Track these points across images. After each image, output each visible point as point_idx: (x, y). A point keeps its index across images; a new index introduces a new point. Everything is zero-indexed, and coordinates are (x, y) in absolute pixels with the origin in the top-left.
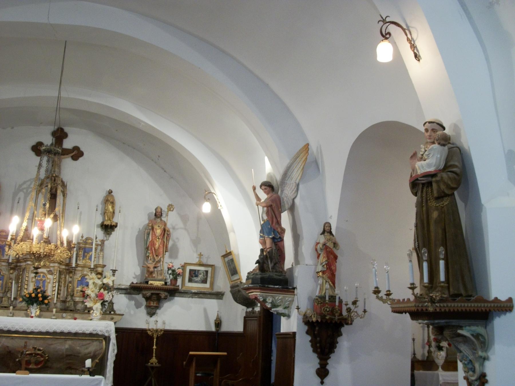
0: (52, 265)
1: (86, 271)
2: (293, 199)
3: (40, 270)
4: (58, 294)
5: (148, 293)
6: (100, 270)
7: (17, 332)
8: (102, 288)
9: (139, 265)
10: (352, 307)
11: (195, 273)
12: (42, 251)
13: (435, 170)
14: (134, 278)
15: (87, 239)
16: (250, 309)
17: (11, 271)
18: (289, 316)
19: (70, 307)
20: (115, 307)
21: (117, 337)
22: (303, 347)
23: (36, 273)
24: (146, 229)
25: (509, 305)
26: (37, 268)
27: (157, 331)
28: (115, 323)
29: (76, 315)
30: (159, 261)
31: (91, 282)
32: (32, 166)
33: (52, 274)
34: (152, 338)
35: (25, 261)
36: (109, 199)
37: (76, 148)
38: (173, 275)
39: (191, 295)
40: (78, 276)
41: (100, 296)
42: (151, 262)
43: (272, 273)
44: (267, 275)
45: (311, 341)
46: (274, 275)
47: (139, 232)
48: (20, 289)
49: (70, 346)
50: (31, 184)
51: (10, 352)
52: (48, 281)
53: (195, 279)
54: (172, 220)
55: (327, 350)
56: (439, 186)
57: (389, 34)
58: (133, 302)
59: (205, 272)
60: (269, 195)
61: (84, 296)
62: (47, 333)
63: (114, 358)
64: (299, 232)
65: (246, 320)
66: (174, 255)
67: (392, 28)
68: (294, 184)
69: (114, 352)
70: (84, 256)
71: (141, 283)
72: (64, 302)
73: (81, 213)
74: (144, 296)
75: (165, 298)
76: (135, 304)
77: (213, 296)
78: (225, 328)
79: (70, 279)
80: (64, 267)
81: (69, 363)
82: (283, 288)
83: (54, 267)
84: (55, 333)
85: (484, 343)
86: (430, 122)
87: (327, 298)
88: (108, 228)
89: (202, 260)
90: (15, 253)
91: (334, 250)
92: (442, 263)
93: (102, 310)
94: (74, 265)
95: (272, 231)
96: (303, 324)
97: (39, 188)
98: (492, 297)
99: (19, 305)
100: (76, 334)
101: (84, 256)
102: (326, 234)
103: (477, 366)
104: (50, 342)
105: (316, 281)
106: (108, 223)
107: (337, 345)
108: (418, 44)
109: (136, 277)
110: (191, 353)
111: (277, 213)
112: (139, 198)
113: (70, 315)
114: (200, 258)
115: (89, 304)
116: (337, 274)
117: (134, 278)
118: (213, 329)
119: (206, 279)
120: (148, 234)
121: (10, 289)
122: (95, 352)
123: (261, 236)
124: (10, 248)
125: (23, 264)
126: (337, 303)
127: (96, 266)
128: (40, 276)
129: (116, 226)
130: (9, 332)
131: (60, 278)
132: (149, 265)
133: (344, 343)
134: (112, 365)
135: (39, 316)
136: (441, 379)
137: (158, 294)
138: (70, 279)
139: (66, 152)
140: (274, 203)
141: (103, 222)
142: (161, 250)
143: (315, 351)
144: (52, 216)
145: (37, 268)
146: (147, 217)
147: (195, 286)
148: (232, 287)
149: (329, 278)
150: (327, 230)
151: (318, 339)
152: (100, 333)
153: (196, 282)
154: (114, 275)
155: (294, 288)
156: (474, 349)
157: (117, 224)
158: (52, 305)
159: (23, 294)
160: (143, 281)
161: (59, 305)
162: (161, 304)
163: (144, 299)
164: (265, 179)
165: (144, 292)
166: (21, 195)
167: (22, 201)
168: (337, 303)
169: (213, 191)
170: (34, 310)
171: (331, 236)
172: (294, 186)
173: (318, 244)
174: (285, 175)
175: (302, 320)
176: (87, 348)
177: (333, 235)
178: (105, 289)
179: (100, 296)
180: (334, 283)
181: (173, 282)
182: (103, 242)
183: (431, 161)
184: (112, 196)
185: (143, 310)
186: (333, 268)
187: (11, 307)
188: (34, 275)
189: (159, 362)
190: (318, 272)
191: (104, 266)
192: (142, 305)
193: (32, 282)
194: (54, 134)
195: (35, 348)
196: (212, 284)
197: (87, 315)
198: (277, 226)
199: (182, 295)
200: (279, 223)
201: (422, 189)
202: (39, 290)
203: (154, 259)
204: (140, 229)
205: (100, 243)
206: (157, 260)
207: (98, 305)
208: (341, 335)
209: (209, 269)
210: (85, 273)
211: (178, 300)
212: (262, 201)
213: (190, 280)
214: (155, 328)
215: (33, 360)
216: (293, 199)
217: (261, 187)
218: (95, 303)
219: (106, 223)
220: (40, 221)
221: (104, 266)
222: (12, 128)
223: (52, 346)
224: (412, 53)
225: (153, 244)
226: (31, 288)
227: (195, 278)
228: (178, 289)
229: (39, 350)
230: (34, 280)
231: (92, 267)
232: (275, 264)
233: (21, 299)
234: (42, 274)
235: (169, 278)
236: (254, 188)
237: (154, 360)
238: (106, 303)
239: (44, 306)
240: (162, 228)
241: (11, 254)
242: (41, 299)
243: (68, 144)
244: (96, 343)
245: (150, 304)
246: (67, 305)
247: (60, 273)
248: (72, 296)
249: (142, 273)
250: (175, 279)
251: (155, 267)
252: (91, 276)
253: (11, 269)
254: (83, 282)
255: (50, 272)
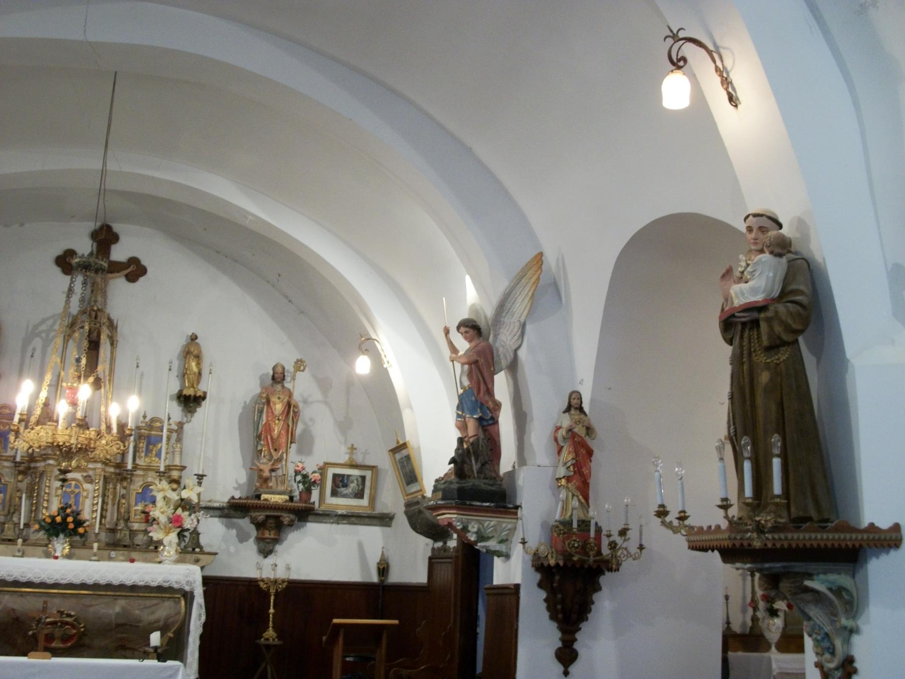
0: (91, 466)
1: (151, 477)
2: (516, 351)
3: (69, 476)
4: (102, 516)
5: (261, 516)
6: (175, 474)
7: (29, 584)
8: (179, 506)
9: (244, 466)
10: (619, 540)
11: (342, 481)
12: (73, 441)
13: (765, 300)
14: (236, 489)
15: (153, 420)
16: (439, 544)
17: (20, 477)
18: (507, 556)
19: (123, 541)
20: (203, 540)
21: (205, 593)
22: (533, 610)
23: (64, 480)
24: (256, 403)
25: (894, 536)
26: (64, 472)
27: (275, 582)
28: (202, 568)
29: (134, 555)
30: (279, 460)
31: (159, 497)
32: (57, 293)
33: (91, 482)
34: (266, 594)
35: (45, 460)
36: (191, 350)
37: (134, 261)
38: (304, 483)
39: (335, 519)
40: (137, 486)
41: (176, 521)
42: (265, 460)
43: (478, 480)
44: (469, 483)
45: (546, 600)
46: (482, 484)
47: (245, 407)
48: (34, 509)
49: (123, 608)
50: (54, 324)
51: (17, 619)
52: (85, 494)
53: (343, 490)
54: (302, 386)
55: (574, 616)
56: (771, 328)
57: (684, 59)
58: (234, 532)
59: (360, 479)
60: (473, 344)
61: (147, 521)
62: (83, 586)
63: (200, 631)
64: (525, 408)
65: (433, 562)
66: (306, 449)
67: (689, 50)
68: (517, 324)
69: (200, 620)
70: (148, 451)
71: (247, 498)
72: (113, 531)
73: (142, 375)
74: (253, 521)
75: (291, 525)
76: (238, 536)
77: (375, 521)
78: (395, 577)
79: (123, 492)
80: (112, 470)
81: (121, 639)
82: (497, 507)
83: (95, 469)
84: (96, 586)
85: (850, 603)
86: (755, 215)
87: (575, 525)
88: (190, 401)
89: (354, 457)
90: (26, 446)
91: (587, 439)
92: (776, 463)
93: (179, 544)
94: (130, 466)
95: (477, 406)
96: (533, 570)
97: (69, 331)
98: (865, 523)
99: (34, 537)
100: (134, 588)
101: (148, 451)
102: (573, 411)
103: (838, 643)
104: (87, 601)
105: (556, 495)
106: (189, 392)
107: (593, 607)
108: (734, 77)
109: (239, 487)
110: (336, 621)
111: (486, 374)
112: (244, 348)
113: (123, 555)
114: (351, 453)
115: (156, 535)
116: (592, 481)
117: (236, 489)
118: (375, 579)
119: (363, 490)
120: (261, 412)
121: (18, 509)
122: (167, 619)
123: (458, 416)
124: (17, 437)
125: (41, 465)
126: (592, 534)
127: (169, 468)
128: (70, 486)
129: (204, 398)
130: (16, 583)
131: (105, 489)
132: (262, 467)
133: (605, 604)
134: (198, 643)
135: (69, 556)
136: (774, 666)
137: (278, 517)
138: (123, 492)
139: (116, 268)
140: (482, 356)
141: (181, 391)
142: (283, 440)
143: (553, 617)
144: (91, 379)
145: (64, 472)
146: (259, 382)
147: (343, 504)
148: (408, 505)
149: (578, 488)
150: (574, 405)
151: (559, 596)
152: (176, 586)
153: (345, 496)
154: (200, 484)
155: (517, 507)
156: (833, 615)
157: (205, 393)
158: (92, 537)
159: (41, 517)
160: (251, 494)
161: (103, 536)
162: (283, 535)
163: (253, 527)
164: (465, 315)
165: (254, 514)
166: (38, 343)
167: (38, 353)
168: (592, 534)
169: (374, 337)
170: (61, 545)
171: (582, 416)
172: (516, 328)
173: (558, 428)
174: (502, 308)
175: (530, 563)
176: (153, 613)
177: (585, 413)
178: (184, 509)
179: (176, 521)
180: (586, 498)
181: (304, 496)
182: (181, 425)
183: (757, 284)
184: (198, 344)
185: (251, 546)
186: (585, 471)
187: (20, 541)
188: (59, 484)
189: (279, 637)
190: (558, 479)
191: (183, 468)
192: (250, 537)
193: (57, 496)
194: (94, 235)
195: (62, 613)
196: (373, 500)
197: (153, 555)
198: (487, 398)
199: (320, 519)
200: (490, 392)
201: (742, 332)
202: (68, 511)
203: (271, 456)
204: (245, 402)
205: (176, 428)
206: (275, 457)
207: (173, 537)
208: (600, 589)
209: (368, 474)
210: (150, 480)
211: (313, 528)
212: (461, 353)
213: (334, 493)
214: (272, 577)
215: (58, 632)
216: (516, 351)
217: (458, 328)
218: (167, 533)
219: (187, 392)
220: (71, 388)
221: (183, 468)
222: (22, 225)
223: (92, 609)
224: (725, 93)
225: (268, 429)
226: (55, 507)
227: (342, 489)
228: (313, 509)
229: (69, 616)
230: (60, 492)
231: (162, 469)
232: (483, 465)
233: (37, 526)
234: (73, 483)
235: (297, 489)
236: (447, 332)
237: (270, 633)
238: (187, 534)
239: (77, 538)
240: (285, 400)
241: (20, 446)
242: (71, 526)
243: (119, 253)
244: (168, 604)
245: (263, 534)
246: (118, 536)
247: (106, 480)
248: (127, 520)
249: (250, 480)
250: (308, 491)
251: (272, 470)
252: (160, 486)
253: (20, 472)
254: (146, 495)
255: (89, 479)
